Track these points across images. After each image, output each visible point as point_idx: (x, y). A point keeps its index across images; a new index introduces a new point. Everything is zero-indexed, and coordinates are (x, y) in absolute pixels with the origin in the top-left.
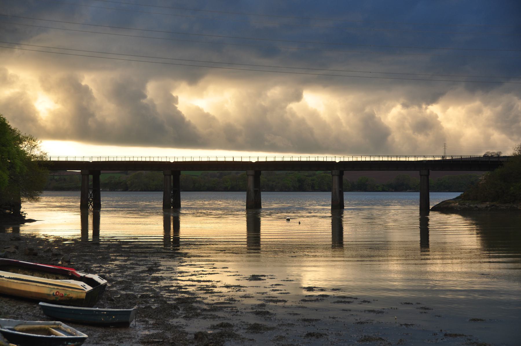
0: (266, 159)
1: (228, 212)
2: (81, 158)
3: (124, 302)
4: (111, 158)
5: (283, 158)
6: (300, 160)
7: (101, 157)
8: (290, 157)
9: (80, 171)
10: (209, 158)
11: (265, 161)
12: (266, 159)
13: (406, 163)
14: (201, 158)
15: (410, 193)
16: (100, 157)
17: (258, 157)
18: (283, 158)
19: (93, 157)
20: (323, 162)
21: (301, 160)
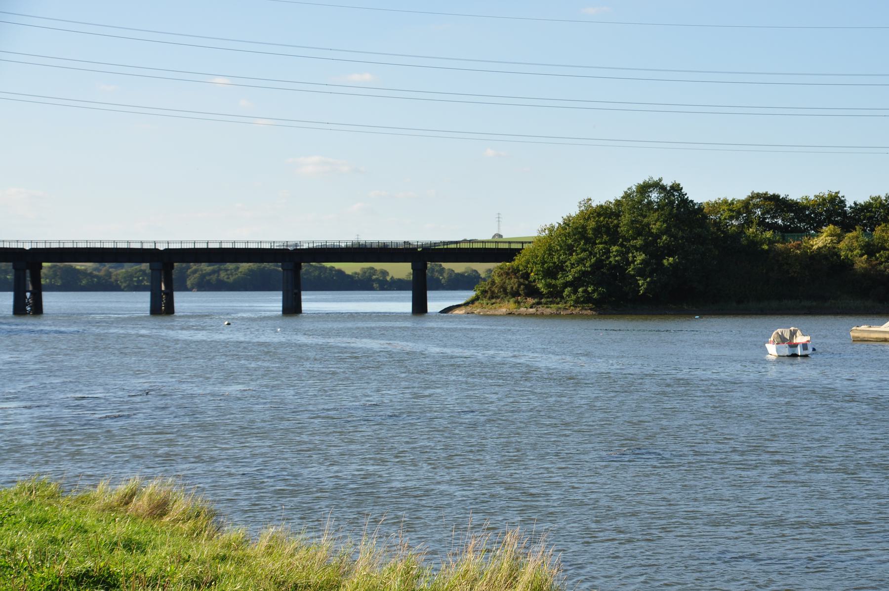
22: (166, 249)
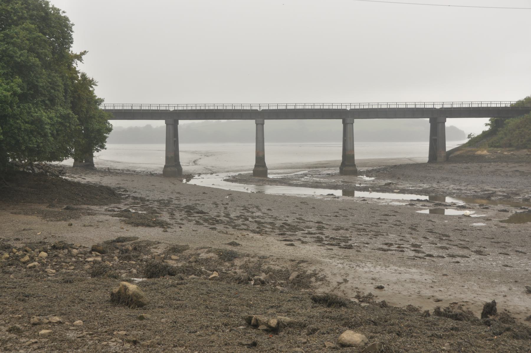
0: (132, 108)
8: (469, 103)
12: (415, 106)
14: (234, 107)
16: (500, 103)
22: (441, 108)
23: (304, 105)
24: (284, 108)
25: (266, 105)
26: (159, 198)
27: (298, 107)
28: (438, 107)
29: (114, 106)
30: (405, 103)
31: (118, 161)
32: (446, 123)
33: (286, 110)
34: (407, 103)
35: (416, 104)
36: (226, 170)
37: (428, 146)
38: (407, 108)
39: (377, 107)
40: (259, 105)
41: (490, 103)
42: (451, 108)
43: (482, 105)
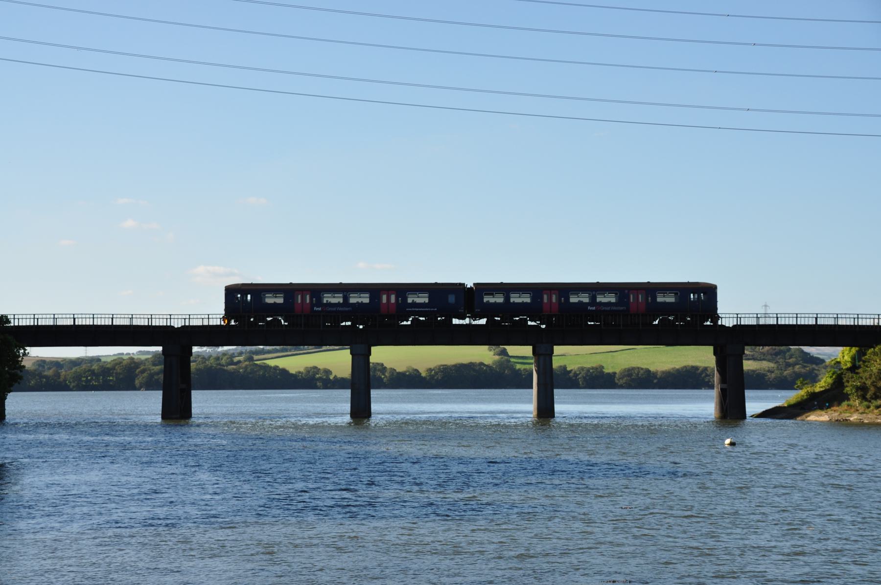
1: (705, 399)
2: (165, 320)
3: (238, 429)
4: (176, 320)
5: (150, 320)
6: (169, 324)
7: (839, 316)
8: (184, 317)
9: (160, 349)
10: (36, 320)
11: (128, 324)
13: (757, 329)
15: (107, 354)
17: (815, 316)
18: (150, 320)
19: (191, 317)
20: (203, 327)
21: (191, 324)
22: (182, 327)
23: (835, 316)
24: (812, 322)
25: (48, 316)
26: (471, 455)
27: (136, 322)
28: (177, 324)
29: (777, 318)
30: (755, 316)
31: (429, 411)
32: (370, 357)
33: (816, 326)
34: (56, 316)
35: (56, 316)
36: (662, 416)
37: (193, 405)
38: (741, 326)
39: (795, 323)
40: (736, 316)
41: (207, 316)
42: (835, 326)
43: (211, 320)
